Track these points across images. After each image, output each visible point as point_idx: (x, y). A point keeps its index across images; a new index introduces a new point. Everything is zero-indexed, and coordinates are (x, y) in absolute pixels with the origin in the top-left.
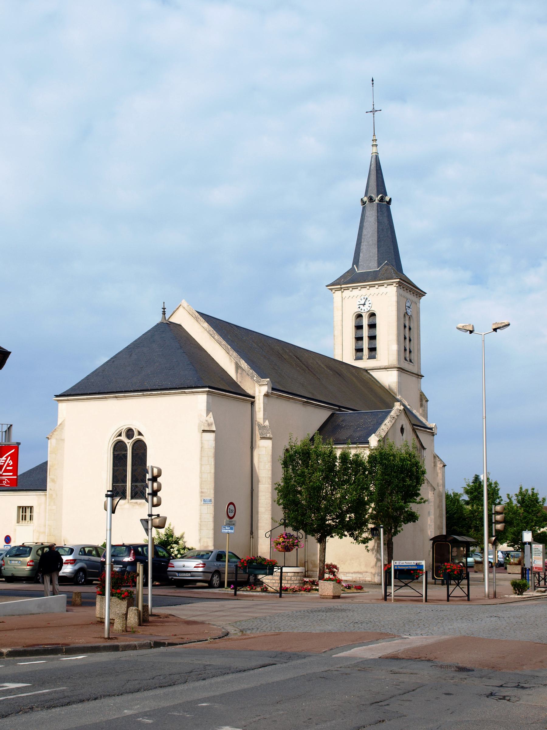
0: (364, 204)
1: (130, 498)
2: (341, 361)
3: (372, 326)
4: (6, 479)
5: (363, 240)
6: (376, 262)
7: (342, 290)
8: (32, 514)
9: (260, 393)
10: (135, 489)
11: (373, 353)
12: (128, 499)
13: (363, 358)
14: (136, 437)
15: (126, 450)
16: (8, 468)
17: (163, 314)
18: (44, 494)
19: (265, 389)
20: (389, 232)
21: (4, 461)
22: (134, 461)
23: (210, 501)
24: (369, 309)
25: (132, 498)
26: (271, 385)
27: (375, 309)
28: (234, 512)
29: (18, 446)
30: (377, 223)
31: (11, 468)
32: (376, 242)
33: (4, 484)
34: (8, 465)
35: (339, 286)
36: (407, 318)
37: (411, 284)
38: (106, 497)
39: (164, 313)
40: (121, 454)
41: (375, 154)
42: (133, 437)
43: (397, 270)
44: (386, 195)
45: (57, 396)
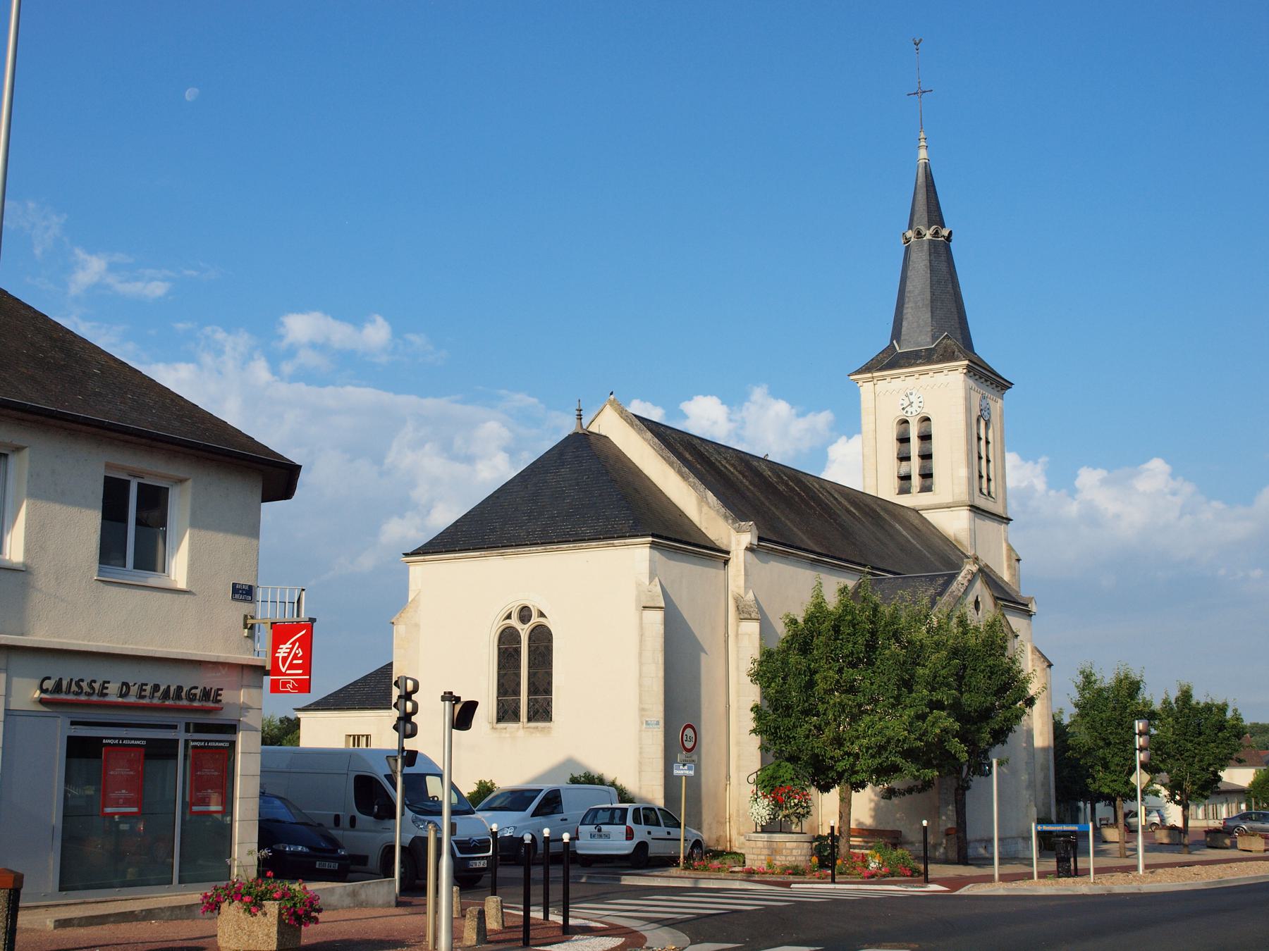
1: (526, 720)
2: (875, 495)
3: (926, 437)
5: (907, 300)
7: (875, 381)
9: (738, 545)
10: (534, 705)
11: (928, 481)
12: (523, 722)
14: (535, 620)
15: (519, 642)
16: (295, 662)
17: (578, 419)
18: (387, 714)
19: (747, 538)
20: (950, 286)
23: (656, 724)
24: (919, 410)
25: (529, 720)
27: (927, 412)
31: (300, 662)
32: (928, 302)
33: (289, 689)
37: (987, 367)
38: (442, 701)
39: (580, 417)
40: (510, 648)
41: (924, 161)
42: (529, 620)
44: (943, 226)
45: (406, 555)
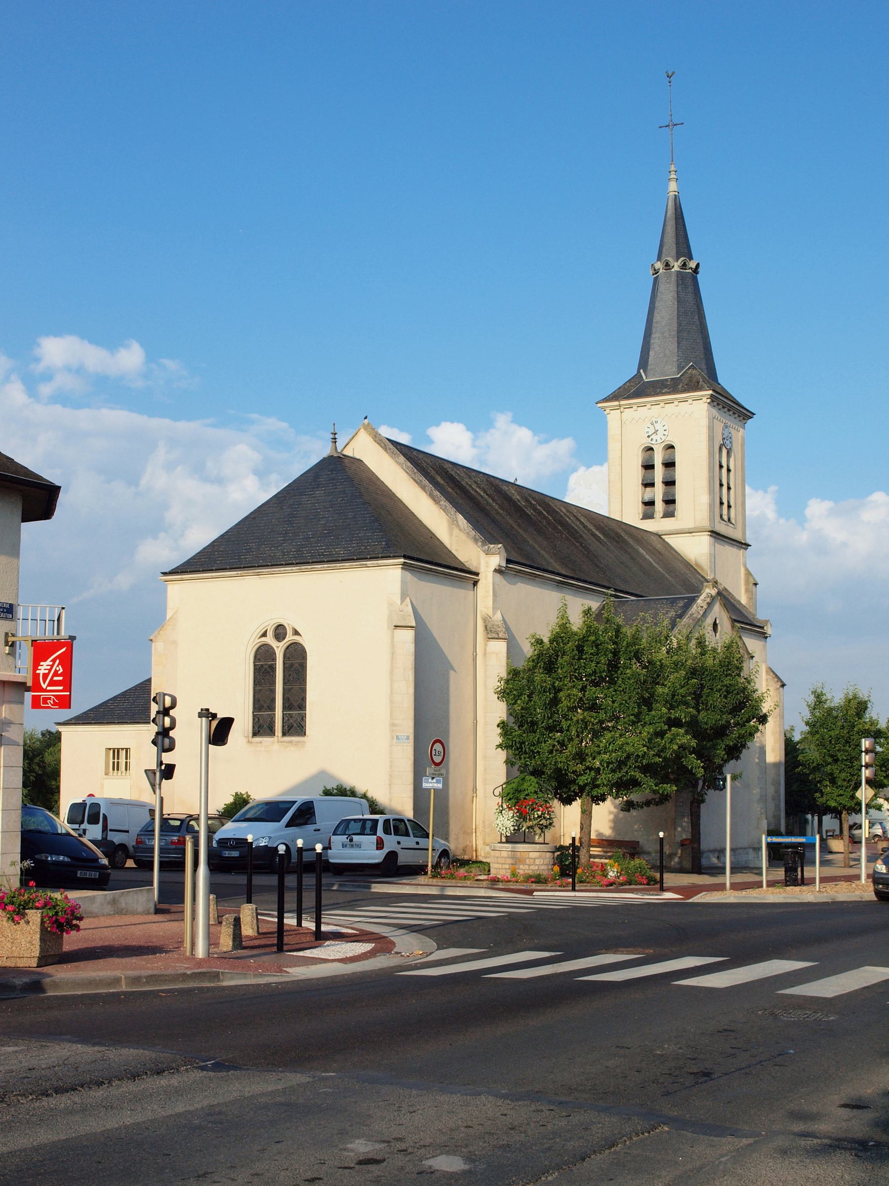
0: (656, 273)
2: (621, 520)
3: (670, 465)
4: (52, 697)
6: (675, 364)
8: (128, 761)
10: (288, 720)
11: (671, 507)
12: (278, 736)
13: (655, 516)
14: (290, 638)
15: (274, 659)
16: (55, 678)
21: (49, 667)
22: (288, 676)
24: (664, 437)
25: (284, 734)
26: (504, 554)
27: (671, 440)
28: (442, 754)
29: (72, 641)
30: (676, 303)
31: (61, 678)
32: (674, 333)
33: (50, 705)
34: (56, 674)
35: (616, 403)
36: (724, 452)
39: (334, 441)
41: (674, 193)
42: (284, 638)
43: (709, 377)
45: (165, 574)
